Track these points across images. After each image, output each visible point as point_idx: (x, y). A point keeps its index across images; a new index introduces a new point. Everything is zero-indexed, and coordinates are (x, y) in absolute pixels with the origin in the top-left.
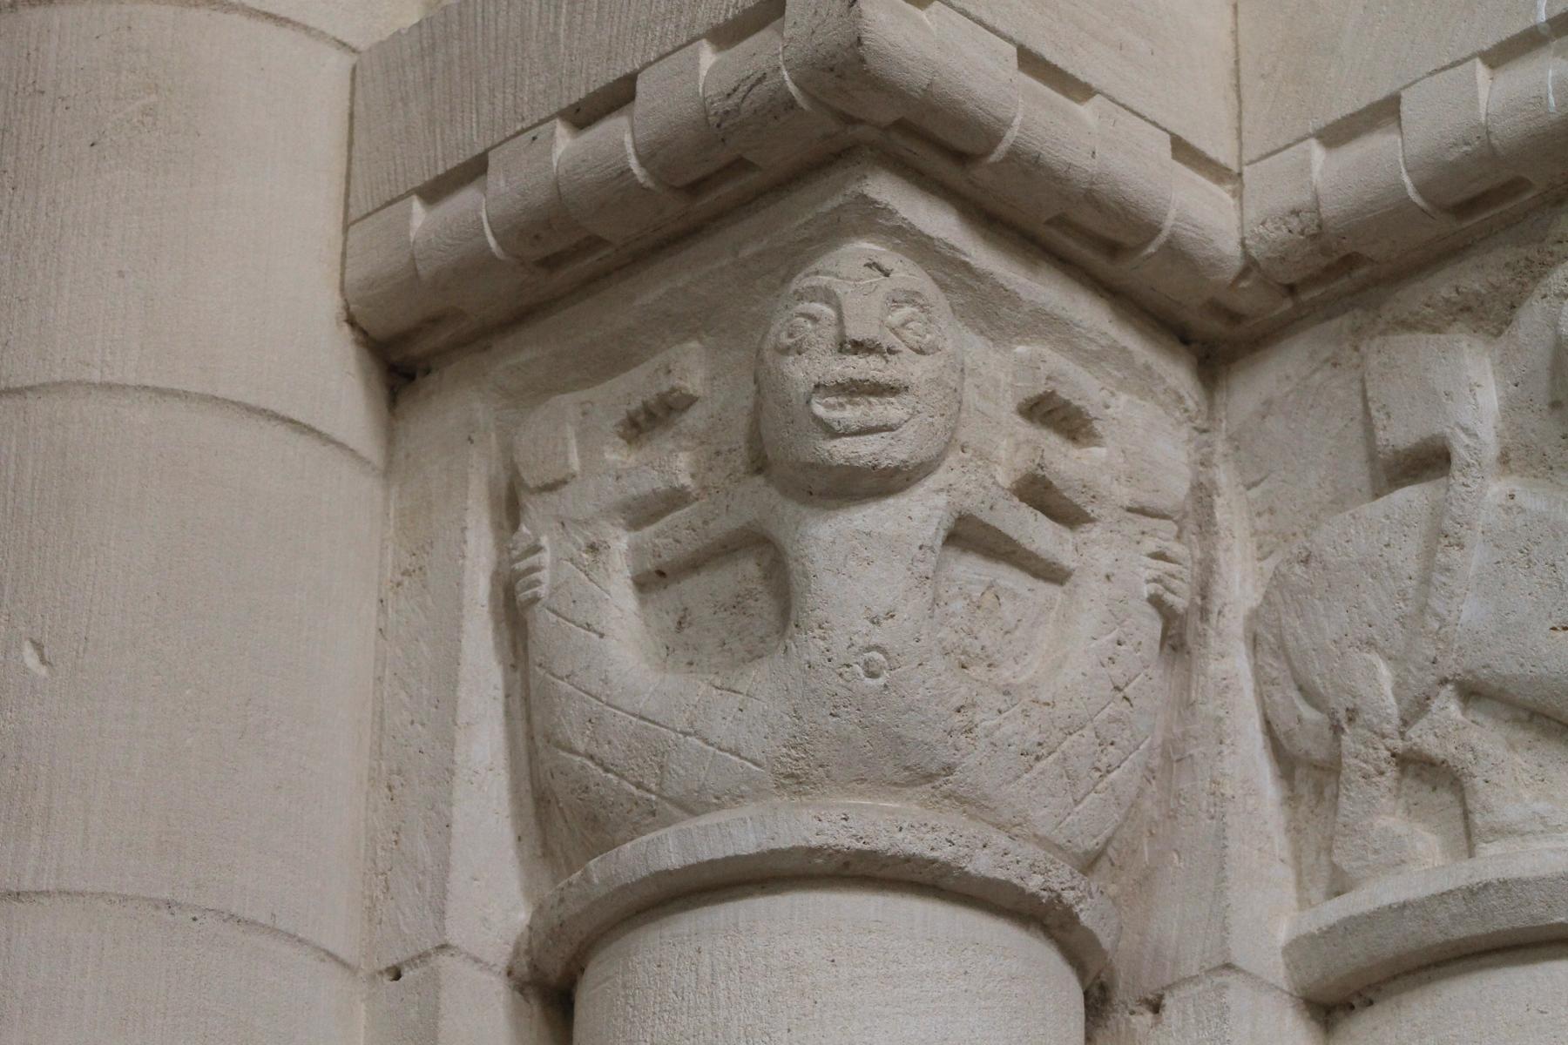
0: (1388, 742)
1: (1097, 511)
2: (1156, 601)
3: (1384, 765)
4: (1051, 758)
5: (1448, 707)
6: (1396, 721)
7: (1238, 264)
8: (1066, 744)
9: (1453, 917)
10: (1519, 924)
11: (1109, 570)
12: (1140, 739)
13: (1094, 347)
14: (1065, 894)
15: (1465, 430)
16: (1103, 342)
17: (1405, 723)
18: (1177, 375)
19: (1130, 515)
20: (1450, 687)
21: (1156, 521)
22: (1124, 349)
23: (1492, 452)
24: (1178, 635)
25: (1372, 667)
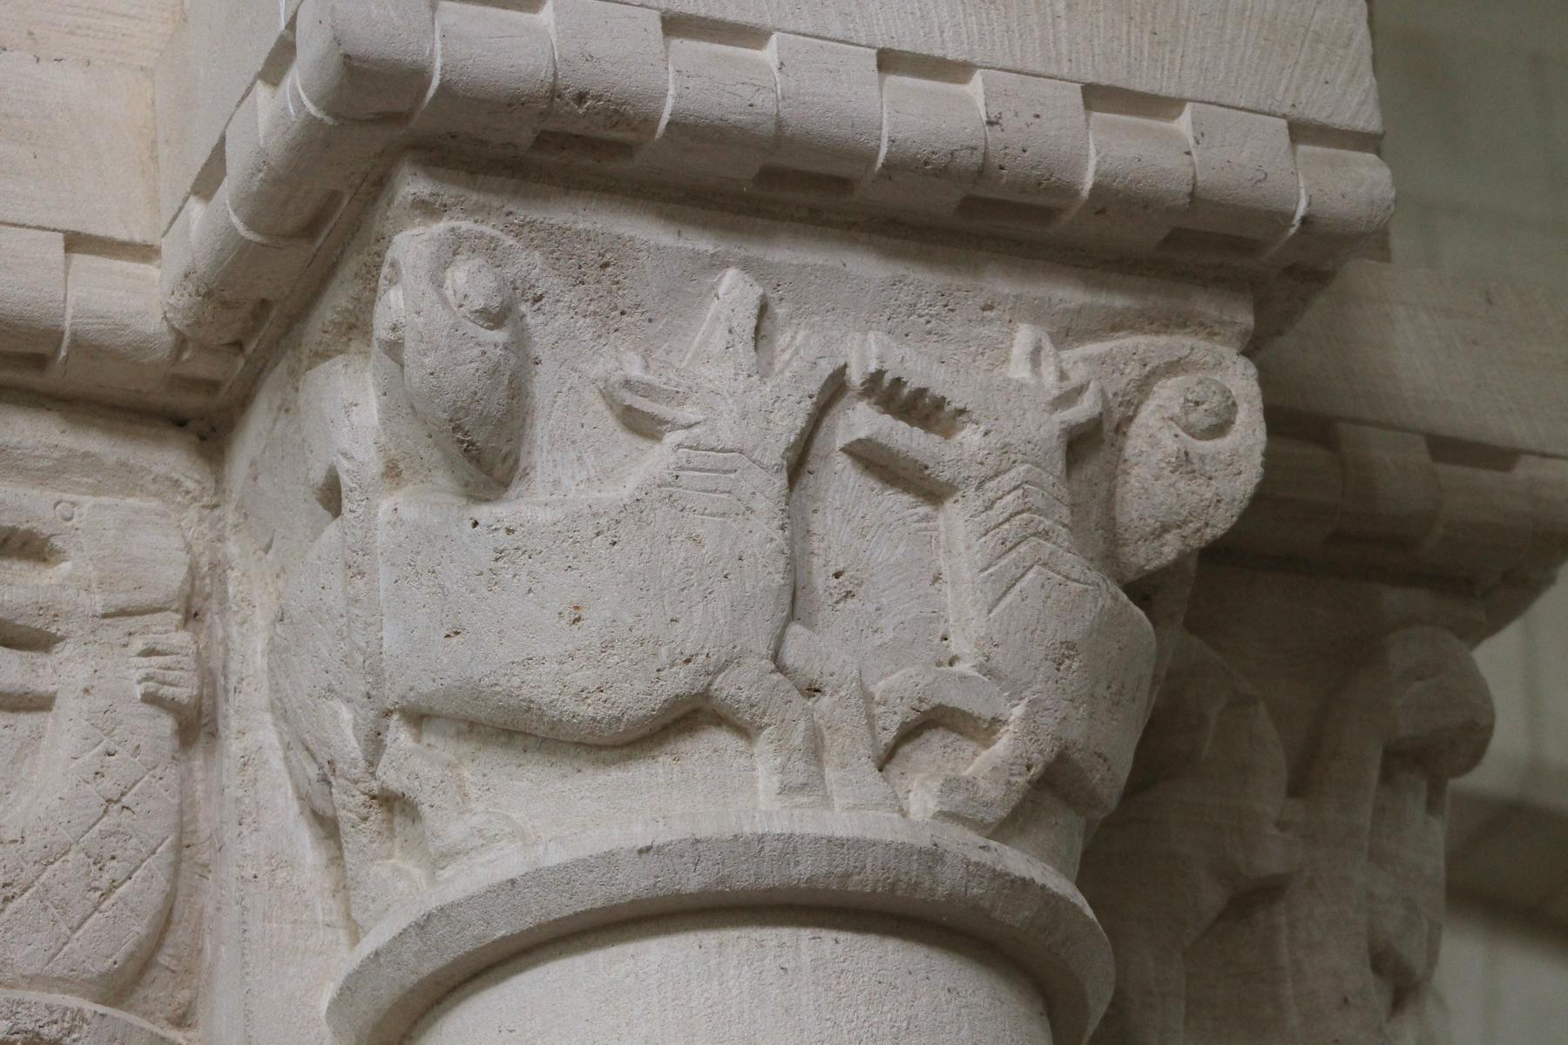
0: (362, 786)
1: (63, 628)
2: (150, 699)
3: (364, 811)
4: (27, 895)
5: (400, 737)
6: (362, 764)
7: (169, 339)
8: (43, 878)
9: (415, 954)
10: (469, 948)
11: (86, 684)
12: (153, 843)
13: (47, 463)
14: (45, 1031)
15: (344, 455)
16: (56, 455)
17: (371, 764)
18: (170, 460)
19: (107, 621)
20: (396, 717)
21: (147, 617)
22: (86, 455)
23: (375, 467)
24: (195, 726)
25: (335, 715)
